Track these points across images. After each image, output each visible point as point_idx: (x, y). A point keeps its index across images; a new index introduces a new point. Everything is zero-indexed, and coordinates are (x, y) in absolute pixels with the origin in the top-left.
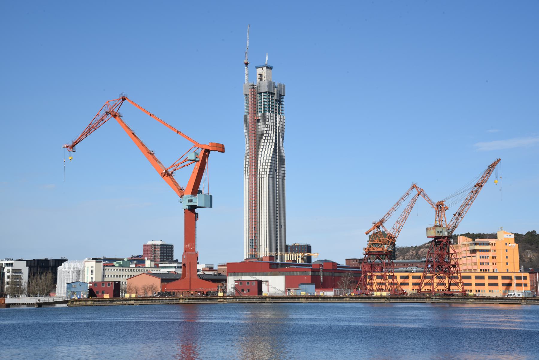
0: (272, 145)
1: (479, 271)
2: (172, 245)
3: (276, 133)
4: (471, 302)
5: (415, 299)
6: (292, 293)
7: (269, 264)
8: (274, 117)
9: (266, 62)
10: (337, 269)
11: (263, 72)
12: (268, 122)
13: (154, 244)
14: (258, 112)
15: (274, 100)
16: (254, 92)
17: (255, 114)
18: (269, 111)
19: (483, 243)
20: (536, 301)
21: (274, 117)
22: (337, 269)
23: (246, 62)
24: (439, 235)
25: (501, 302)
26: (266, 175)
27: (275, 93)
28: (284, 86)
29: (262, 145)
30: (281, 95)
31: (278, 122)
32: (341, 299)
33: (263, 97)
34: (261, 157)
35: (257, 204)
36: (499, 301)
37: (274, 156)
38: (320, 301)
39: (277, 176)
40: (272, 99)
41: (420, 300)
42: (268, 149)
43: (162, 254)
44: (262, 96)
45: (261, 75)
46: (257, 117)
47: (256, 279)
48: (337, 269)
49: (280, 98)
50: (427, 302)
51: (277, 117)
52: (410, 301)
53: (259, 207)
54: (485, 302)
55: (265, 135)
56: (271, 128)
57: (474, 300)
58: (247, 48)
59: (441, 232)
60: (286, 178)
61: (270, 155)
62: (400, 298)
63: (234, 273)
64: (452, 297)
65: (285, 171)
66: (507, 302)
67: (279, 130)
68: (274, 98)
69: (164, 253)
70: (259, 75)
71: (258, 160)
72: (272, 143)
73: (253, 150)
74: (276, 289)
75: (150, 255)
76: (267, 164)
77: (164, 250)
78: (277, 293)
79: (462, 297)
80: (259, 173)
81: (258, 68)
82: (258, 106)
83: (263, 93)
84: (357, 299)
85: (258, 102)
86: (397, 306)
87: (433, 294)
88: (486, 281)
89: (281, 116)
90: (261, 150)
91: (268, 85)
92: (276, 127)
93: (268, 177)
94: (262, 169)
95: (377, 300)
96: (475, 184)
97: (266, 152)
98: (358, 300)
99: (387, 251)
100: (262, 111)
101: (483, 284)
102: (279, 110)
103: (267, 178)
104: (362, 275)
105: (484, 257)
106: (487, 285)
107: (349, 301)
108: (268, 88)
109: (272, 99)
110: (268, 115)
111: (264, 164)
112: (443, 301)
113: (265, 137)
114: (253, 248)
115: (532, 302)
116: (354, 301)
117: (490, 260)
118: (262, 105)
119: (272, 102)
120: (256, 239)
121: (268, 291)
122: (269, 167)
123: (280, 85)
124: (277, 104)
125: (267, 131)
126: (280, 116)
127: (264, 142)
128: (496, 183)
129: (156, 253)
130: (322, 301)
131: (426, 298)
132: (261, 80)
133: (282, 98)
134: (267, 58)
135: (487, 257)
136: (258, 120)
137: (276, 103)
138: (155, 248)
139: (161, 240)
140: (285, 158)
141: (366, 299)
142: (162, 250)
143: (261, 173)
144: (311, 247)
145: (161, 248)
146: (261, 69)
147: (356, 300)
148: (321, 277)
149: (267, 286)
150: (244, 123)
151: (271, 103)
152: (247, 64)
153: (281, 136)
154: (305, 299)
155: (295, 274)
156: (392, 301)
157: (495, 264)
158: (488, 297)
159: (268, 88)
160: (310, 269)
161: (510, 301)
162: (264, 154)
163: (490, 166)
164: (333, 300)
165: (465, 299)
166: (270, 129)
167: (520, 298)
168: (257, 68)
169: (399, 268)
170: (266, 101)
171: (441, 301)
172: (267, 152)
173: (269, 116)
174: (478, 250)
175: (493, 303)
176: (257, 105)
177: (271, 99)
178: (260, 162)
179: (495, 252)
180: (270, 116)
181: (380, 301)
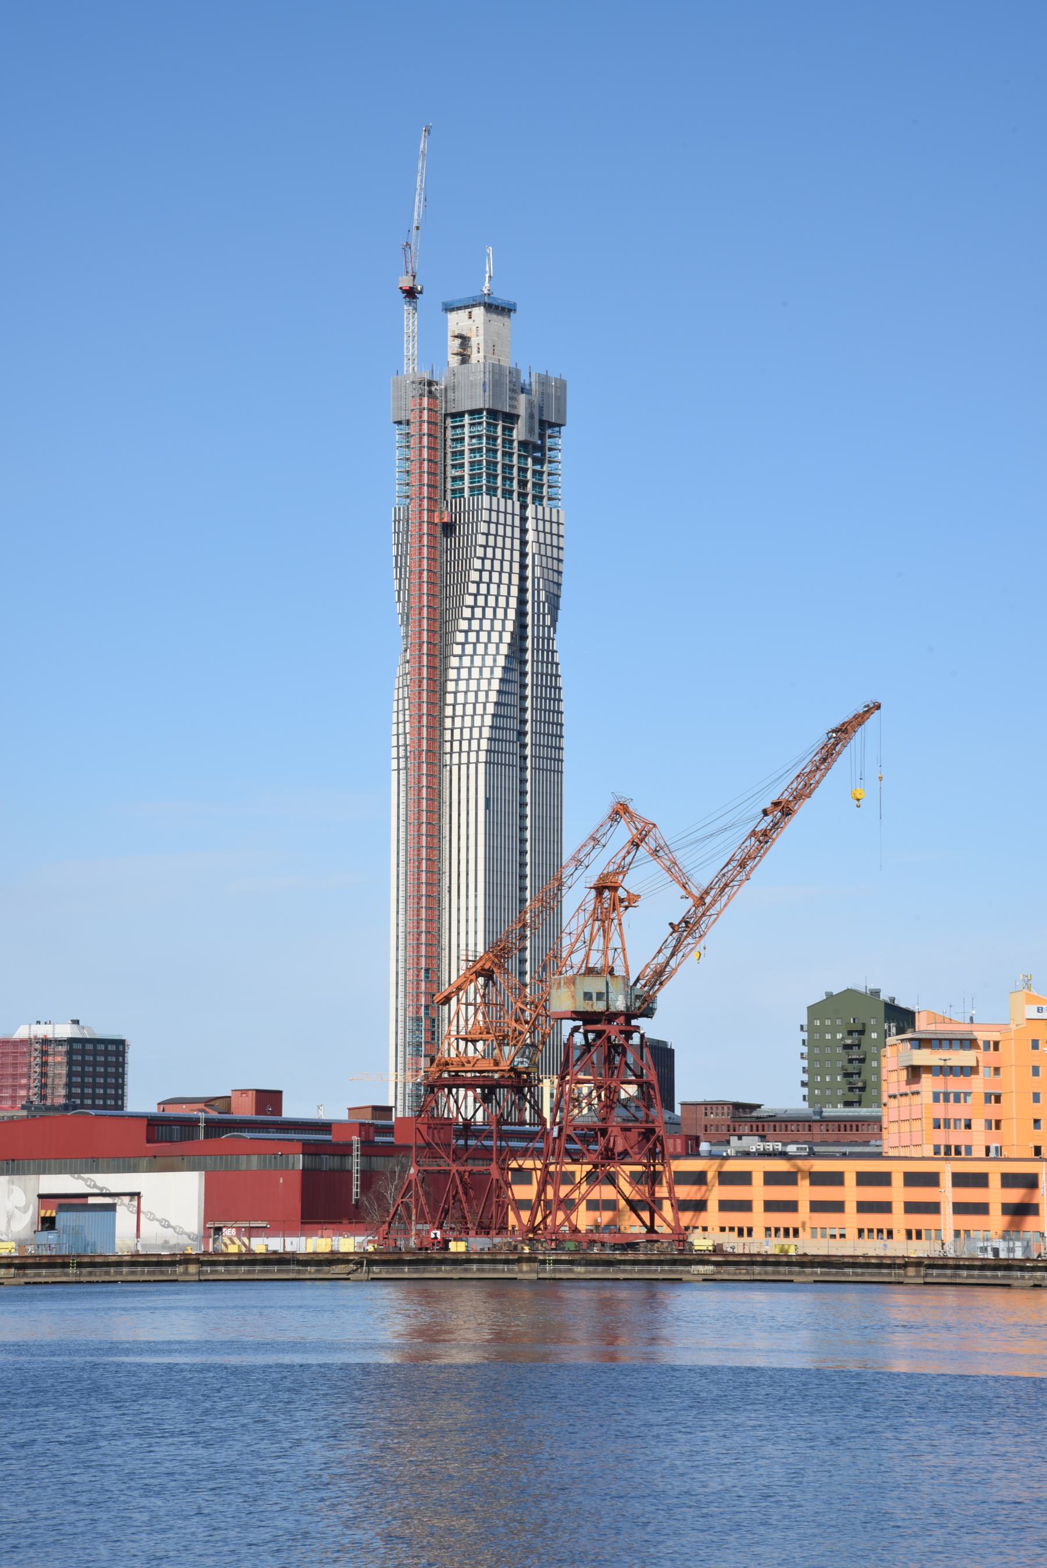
0: (504, 629)
1: (929, 1152)
2: (121, 1043)
3: (523, 578)
4: (701, 1278)
5: (475, 1267)
6: (232, 1242)
7: (145, 1123)
8: (513, 514)
9: (487, 284)
10: (373, 1142)
11: (474, 328)
12: (487, 535)
13: (40, 1036)
14: (449, 493)
15: (515, 444)
16: (429, 410)
17: (436, 501)
18: (492, 491)
19: (950, 1040)
20: (965, 1273)
21: (513, 514)
22: (377, 1139)
23: (406, 282)
24: (589, 1009)
25: (822, 1274)
26: (469, 753)
27: (518, 416)
28: (562, 386)
29: (461, 631)
30: (544, 424)
31: (530, 536)
32: (164, 1269)
33: (466, 430)
34: (457, 681)
35: (440, 872)
36: (816, 1273)
37: (515, 676)
38: (78, 1279)
39: (525, 758)
40: (508, 442)
41: (495, 1271)
42: (486, 645)
43: (74, 1079)
44: (463, 426)
45: (464, 340)
46: (441, 512)
47: (95, 1186)
48: (377, 1139)
49: (542, 437)
50: (520, 1276)
51: (530, 512)
52: (451, 1271)
53: (450, 887)
54: (760, 1274)
55: (472, 588)
56: (502, 561)
57: (710, 1268)
58: (415, 224)
59: (600, 996)
60: (566, 767)
61: (492, 672)
62: (410, 1263)
63: (13, 1160)
64: (623, 1258)
65: (561, 737)
66: (844, 1274)
67: (538, 570)
68: (515, 437)
69: (83, 1074)
70: (458, 341)
71: (445, 693)
72: (503, 621)
73: (425, 650)
74: (169, 1226)
75: (24, 1081)
76: (480, 709)
77: (83, 1063)
78: (172, 1242)
79: (662, 1258)
80: (448, 745)
81: (452, 310)
82: (449, 468)
83: (466, 416)
84: (232, 1268)
85: (449, 450)
86: (569, 1295)
87: (553, 1245)
88: (947, 1194)
89: (547, 510)
90: (457, 650)
91: (487, 381)
92: (523, 555)
93: (486, 763)
94: (462, 729)
95: (318, 1271)
96: (768, 805)
97: (478, 661)
98: (237, 1272)
99: (509, 1071)
100: (462, 490)
101: (933, 1208)
102: (538, 486)
103: (482, 767)
104: (412, 1171)
105: (952, 1096)
106: (947, 1209)
107: (196, 1278)
108: (487, 394)
109: (508, 442)
110: (486, 505)
111: (469, 709)
112: (590, 1272)
113: (475, 596)
114: (418, 1055)
115: (945, 1276)
116: (222, 1273)
117: (979, 1112)
118: (462, 466)
119: (504, 454)
120: (435, 1016)
121: (138, 1236)
122: (488, 721)
123: (544, 381)
124: (530, 460)
125: (481, 571)
126: (540, 508)
127: (469, 620)
128: (858, 800)
129: (50, 1074)
130: (82, 1279)
131: (519, 1261)
132: (465, 358)
133: (550, 437)
134: (489, 268)
135: (962, 1095)
136: (448, 529)
137: (526, 458)
138: (46, 1051)
139: (76, 1022)
140: (561, 683)
141: (271, 1268)
142: (77, 1063)
143: (456, 745)
144: (671, 1052)
145: (70, 1053)
146: (463, 314)
147: (228, 1272)
148: (355, 1175)
149: (136, 1215)
150: (393, 538)
151: (499, 454)
152: (411, 293)
153: (543, 594)
154: (12, 1270)
155: (243, 1167)
156: (380, 1272)
157: (998, 1127)
158: (898, 1257)
159: (487, 394)
160: (299, 1147)
161: (859, 1270)
162: (470, 669)
163: (833, 731)
164: (133, 1273)
165: (674, 1262)
166: (497, 564)
167: (898, 1261)
168: (449, 308)
169: (873, 1142)
170: (480, 450)
171: (580, 1273)
172: (483, 660)
173: (490, 510)
174: (928, 1069)
175: (792, 1281)
176: (445, 466)
177: (499, 441)
178: (452, 702)
179: (997, 1078)
180: (498, 512)
181: (329, 1272)
